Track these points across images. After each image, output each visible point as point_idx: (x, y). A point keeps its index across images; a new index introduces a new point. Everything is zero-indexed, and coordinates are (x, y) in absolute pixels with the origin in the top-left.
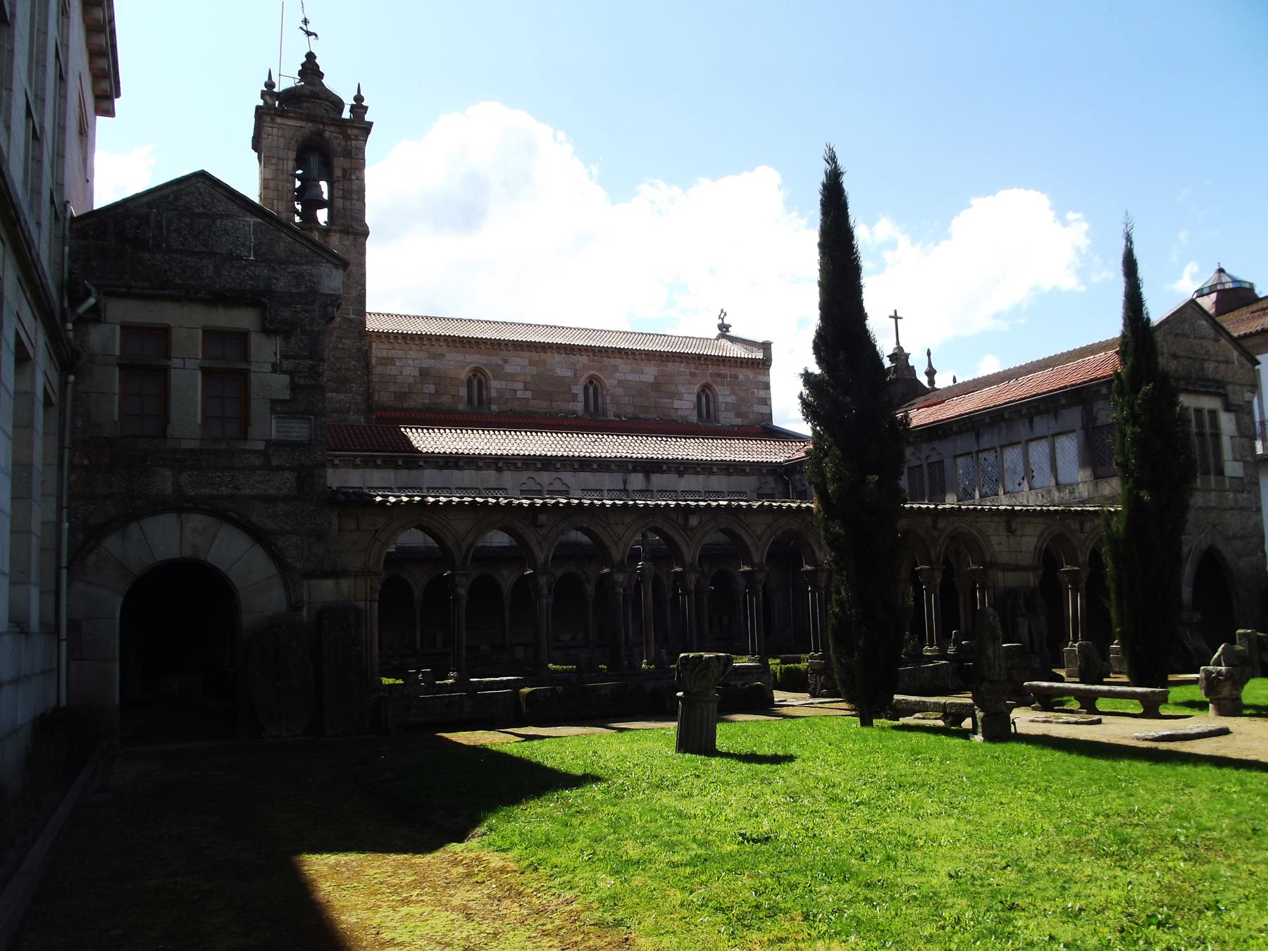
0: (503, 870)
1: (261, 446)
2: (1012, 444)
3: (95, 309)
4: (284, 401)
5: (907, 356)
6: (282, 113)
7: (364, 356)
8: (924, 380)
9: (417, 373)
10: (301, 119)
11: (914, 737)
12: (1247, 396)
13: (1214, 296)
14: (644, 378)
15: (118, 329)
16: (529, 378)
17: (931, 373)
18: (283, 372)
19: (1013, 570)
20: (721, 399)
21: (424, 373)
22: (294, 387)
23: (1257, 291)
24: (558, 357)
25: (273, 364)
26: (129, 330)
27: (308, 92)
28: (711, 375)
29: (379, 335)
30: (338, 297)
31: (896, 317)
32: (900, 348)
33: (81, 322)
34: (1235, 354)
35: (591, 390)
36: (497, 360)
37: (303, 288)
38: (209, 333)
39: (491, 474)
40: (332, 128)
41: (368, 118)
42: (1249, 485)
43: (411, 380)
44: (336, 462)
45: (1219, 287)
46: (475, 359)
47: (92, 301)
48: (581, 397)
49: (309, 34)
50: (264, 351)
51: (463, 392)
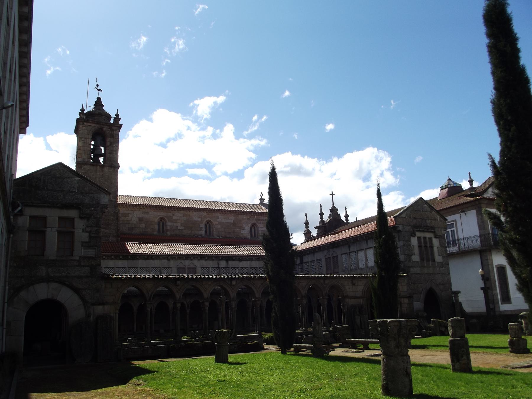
0: (149, 391)
1: (78, 258)
2: (362, 250)
3: (20, 211)
4: (86, 242)
5: (337, 210)
6: (87, 121)
7: (116, 215)
8: (344, 219)
9: (138, 220)
10: (94, 123)
11: (304, 359)
12: (444, 232)
13: (447, 189)
14: (229, 221)
15: (28, 218)
16: (183, 221)
17: (347, 216)
18: (86, 232)
19: (354, 298)
20: (260, 229)
21: (141, 220)
22: (90, 237)
23: (463, 187)
24: (195, 213)
25: (83, 229)
26: (32, 218)
27: (97, 113)
28: (256, 220)
29: (123, 205)
30: (107, 205)
31: (332, 194)
32: (334, 207)
33: (16, 215)
34: (438, 217)
35: (208, 226)
36: (170, 214)
37: (94, 203)
38: (60, 218)
39: (165, 261)
40: (106, 127)
41: (120, 123)
42: (445, 265)
43: (135, 222)
44: (104, 257)
45: (449, 186)
46: (162, 214)
47: (20, 208)
48: (204, 229)
49: (98, 90)
50: (80, 225)
51: (156, 227)
